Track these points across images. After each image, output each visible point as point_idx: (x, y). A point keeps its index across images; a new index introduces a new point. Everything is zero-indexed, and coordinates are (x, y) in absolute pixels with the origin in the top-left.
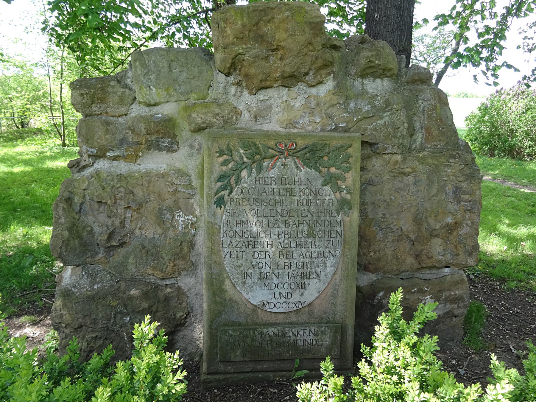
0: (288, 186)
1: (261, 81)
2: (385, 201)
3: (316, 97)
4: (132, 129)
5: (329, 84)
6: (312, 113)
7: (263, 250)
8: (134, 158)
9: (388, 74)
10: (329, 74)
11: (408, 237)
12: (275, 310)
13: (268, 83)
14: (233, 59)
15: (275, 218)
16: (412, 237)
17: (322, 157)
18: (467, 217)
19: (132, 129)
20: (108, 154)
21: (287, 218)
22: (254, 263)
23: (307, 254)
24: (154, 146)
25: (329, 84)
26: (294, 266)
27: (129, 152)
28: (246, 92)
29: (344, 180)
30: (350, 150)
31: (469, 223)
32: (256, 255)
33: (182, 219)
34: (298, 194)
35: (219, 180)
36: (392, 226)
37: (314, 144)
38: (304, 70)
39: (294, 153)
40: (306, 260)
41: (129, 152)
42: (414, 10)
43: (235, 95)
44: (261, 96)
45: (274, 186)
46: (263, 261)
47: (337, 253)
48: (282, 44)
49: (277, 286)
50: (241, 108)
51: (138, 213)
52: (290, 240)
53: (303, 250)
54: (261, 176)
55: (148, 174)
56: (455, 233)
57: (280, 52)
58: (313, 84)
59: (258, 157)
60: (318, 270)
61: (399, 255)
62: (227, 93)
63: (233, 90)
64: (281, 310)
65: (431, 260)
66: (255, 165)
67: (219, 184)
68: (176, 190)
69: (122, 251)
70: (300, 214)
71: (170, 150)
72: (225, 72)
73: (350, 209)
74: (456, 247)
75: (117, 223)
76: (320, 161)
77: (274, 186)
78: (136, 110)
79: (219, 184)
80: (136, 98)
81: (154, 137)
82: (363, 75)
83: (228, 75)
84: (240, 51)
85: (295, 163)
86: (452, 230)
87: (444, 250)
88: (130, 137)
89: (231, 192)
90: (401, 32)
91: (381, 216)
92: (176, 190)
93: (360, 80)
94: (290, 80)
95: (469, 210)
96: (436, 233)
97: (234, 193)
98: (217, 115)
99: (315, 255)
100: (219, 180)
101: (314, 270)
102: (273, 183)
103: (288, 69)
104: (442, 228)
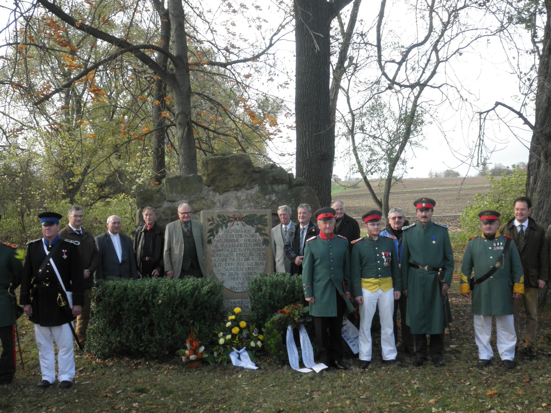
5: (256, 188)
6: (249, 202)
10: (256, 184)
12: (237, 291)
13: (228, 189)
15: (273, 69)
25: (256, 188)
26: (244, 269)
28: (218, 194)
29: (265, 230)
30: (267, 217)
35: (208, 232)
37: (250, 215)
38: (244, 183)
39: (240, 219)
42: (296, 147)
44: (226, 194)
45: (233, 233)
49: (237, 279)
50: (215, 201)
53: (249, 262)
54: (227, 229)
57: (233, 176)
59: (225, 221)
60: (256, 271)
62: (209, 195)
63: (211, 193)
64: (240, 291)
67: (209, 234)
77: (233, 233)
79: (209, 234)
82: (272, 183)
83: (209, 186)
89: (214, 237)
94: (238, 187)
99: (254, 264)
100: (208, 232)
103: (237, 183)
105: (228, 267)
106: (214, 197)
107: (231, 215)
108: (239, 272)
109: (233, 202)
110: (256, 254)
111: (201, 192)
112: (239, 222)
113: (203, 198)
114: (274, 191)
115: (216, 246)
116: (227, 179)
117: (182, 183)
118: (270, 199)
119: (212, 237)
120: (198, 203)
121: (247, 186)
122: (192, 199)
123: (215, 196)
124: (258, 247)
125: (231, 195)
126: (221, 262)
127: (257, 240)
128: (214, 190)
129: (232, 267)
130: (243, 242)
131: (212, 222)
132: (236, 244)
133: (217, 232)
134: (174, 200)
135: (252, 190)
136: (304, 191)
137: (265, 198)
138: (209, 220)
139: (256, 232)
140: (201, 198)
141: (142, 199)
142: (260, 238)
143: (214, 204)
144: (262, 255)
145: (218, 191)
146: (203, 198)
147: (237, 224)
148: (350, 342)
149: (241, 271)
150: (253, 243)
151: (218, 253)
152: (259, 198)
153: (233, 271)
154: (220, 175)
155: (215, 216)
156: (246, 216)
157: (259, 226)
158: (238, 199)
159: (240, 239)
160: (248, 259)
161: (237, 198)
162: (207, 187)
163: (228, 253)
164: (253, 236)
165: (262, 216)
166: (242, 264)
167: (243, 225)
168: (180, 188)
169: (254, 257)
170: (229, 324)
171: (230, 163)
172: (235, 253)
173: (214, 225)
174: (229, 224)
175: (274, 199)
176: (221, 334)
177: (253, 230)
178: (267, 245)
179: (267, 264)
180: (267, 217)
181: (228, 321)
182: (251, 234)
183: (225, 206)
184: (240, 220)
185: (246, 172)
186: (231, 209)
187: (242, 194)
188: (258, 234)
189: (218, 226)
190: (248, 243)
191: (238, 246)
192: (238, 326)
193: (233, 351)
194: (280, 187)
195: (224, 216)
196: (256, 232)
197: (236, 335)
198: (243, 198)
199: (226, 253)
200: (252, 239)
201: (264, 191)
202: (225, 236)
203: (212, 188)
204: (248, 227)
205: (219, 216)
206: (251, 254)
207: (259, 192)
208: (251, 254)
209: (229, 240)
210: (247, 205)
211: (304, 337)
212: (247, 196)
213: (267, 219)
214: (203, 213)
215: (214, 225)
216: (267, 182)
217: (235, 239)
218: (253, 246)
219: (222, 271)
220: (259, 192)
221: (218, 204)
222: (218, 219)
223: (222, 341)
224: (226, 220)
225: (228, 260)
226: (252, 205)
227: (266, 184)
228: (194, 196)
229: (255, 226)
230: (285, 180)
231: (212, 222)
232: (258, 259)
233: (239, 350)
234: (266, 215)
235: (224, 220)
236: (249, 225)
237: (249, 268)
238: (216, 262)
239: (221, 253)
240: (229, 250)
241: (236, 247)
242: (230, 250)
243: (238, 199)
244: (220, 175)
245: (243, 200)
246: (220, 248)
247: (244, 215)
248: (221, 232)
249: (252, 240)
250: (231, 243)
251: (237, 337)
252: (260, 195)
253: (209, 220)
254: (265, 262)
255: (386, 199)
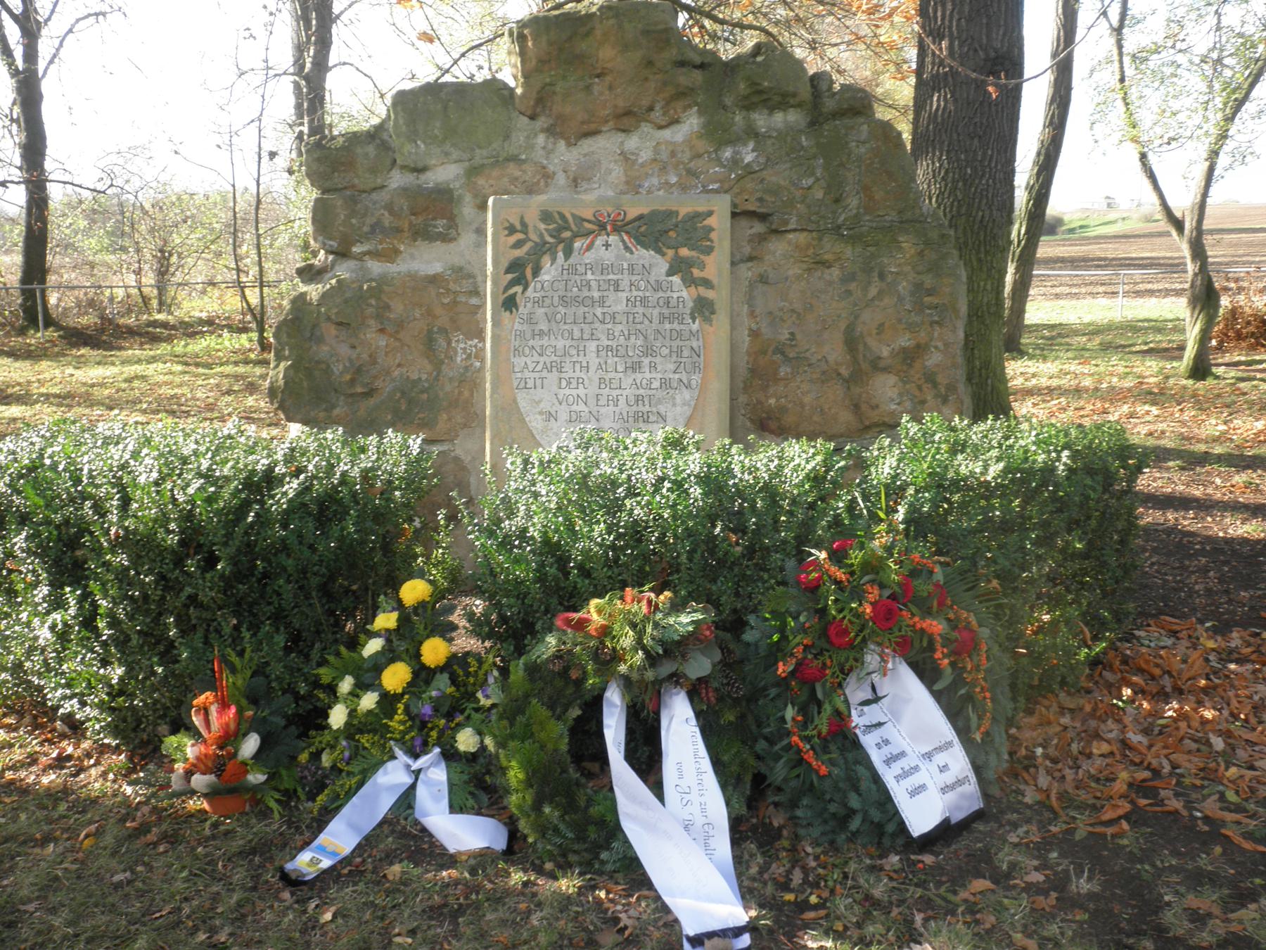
0: (611, 277)
1: (583, 123)
2: (793, 311)
3: (667, 143)
4: (389, 207)
5: (692, 123)
6: (663, 169)
7: (572, 375)
8: (391, 255)
9: (792, 101)
10: (690, 106)
11: (839, 374)
13: (593, 127)
14: (538, 92)
16: (845, 372)
17: (666, 232)
18: (936, 334)
19: (389, 207)
20: (354, 249)
21: (610, 326)
22: (560, 397)
23: (644, 382)
24: (423, 234)
25: (692, 123)
26: (622, 401)
27: (385, 245)
28: (562, 144)
29: (702, 266)
30: (711, 221)
31: (940, 344)
32: (564, 383)
33: (462, 345)
34: (627, 289)
36: (808, 354)
38: (645, 103)
40: (641, 392)
41: (385, 245)
43: (544, 148)
44: (587, 145)
45: (589, 276)
46: (574, 392)
47: (693, 382)
48: (609, 65)
50: (551, 168)
51: (396, 339)
52: (616, 359)
53: (639, 376)
54: (571, 261)
55: (412, 276)
56: (917, 365)
57: (608, 78)
58: (663, 123)
59: (567, 234)
60: (662, 409)
61: (826, 407)
62: (532, 147)
63: (541, 139)
65: (876, 412)
66: (561, 247)
67: (510, 276)
68: (455, 302)
69: (372, 402)
70: (631, 319)
71: (445, 238)
72: (529, 113)
73: (713, 313)
74: (920, 388)
75: (365, 356)
76: (663, 239)
78: (397, 180)
79: (510, 276)
80: (395, 161)
81: (420, 219)
82: (748, 105)
84: (548, 80)
85: (623, 241)
86: (913, 360)
87: (901, 395)
88: (387, 220)
89: (525, 289)
90: (989, 17)
91: (788, 336)
92: (455, 302)
93: (744, 113)
94: (627, 119)
95: (937, 322)
96: (882, 364)
97: (530, 289)
98: (516, 179)
99: (656, 384)
101: (654, 410)
102: (589, 272)
103: (621, 103)
104: (894, 355)
105: (567, 392)
106: (549, 152)
107: (588, 214)
108: (603, 410)
109: (609, 172)
110: (665, 351)
111: (507, 137)
112: (613, 239)
113: (514, 159)
114: (752, 133)
115: (530, 320)
116: (588, 88)
117: (445, 108)
118: (736, 162)
119: (518, 289)
120: (495, 173)
121: (657, 115)
122: (478, 160)
123: (552, 151)
124: (676, 326)
125: (605, 145)
126: (545, 374)
127: (673, 302)
128: (550, 131)
129: (581, 391)
130: (621, 307)
131: (521, 236)
132: (599, 311)
133: (536, 272)
134: (420, 165)
135: (675, 128)
136: (864, 136)
137: (718, 160)
138: (512, 230)
139: (670, 273)
140: (508, 160)
141: (318, 160)
142: (685, 294)
143: (548, 176)
144: (686, 353)
145: (562, 135)
146: (514, 159)
147: (607, 245)
148: (898, 778)
149: (611, 408)
150: (656, 312)
151: (536, 343)
152: (699, 156)
153: (581, 407)
154: (564, 78)
155: (533, 218)
156: (640, 217)
157: (684, 252)
158: (627, 159)
159: (612, 296)
160: (635, 367)
161: (626, 158)
162: (526, 120)
163: (568, 343)
164: (658, 287)
165: (696, 217)
166: (615, 384)
167: (627, 248)
168: (438, 124)
169: (658, 360)
170: (373, 646)
171: (598, 33)
172: (592, 346)
173: (526, 248)
174: (577, 245)
175: (749, 158)
176: (346, 685)
177: (662, 265)
178: (707, 320)
179: (703, 388)
180: (711, 221)
181: (372, 635)
182: (652, 279)
183: (585, 185)
184: (617, 229)
185: (650, 63)
186: (592, 200)
187: (642, 143)
188: (676, 279)
189: (542, 249)
190: (640, 310)
191: (603, 322)
192: (414, 657)
193: (393, 757)
194: (779, 118)
195: (562, 216)
196: (670, 273)
197: (397, 697)
198: (645, 155)
199: (560, 344)
200: (653, 297)
201: (717, 134)
202: (561, 286)
203: (542, 122)
204: (645, 255)
205: (546, 217)
206: (649, 351)
207: (700, 136)
208: (649, 351)
209: (575, 299)
210: (655, 181)
211: (680, 729)
212: (656, 149)
213: (711, 229)
214: (495, 200)
215: (526, 248)
216: (728, 101)
217: (596, 294)
218: (656, 321)
219: (545, 406)
220: (700, 136)
221: (561, 179)
222: (542, 226)
223: (338, 717)
224: (568, 228)
225: (567, 367)
226: (674, 180)
227: (725, 108)
228: (484, 153)
229: (670, 253)
230: (794, 95)
231: (521, 236)
232: (672, 367)
233: (416, 757)
234: (710, 213)
235: (560, 229)
236: (646, 247)
237: (638, 399)
238: (527, 374)
239: (545, 342)
240: (571, 333)
241: (597, 325)
242: (577, 334)
243: (627, 159)
244: (564, 78)
245: (642, 165)
246: (543, 326)
247: (633, 213)
248: (549, 272)
249: (653, 300)
250: (582, 309)
251: (401, 707)
252: (702, 145)
253: (512, 230)
254: (696, 379)
255: (1196, 212)
